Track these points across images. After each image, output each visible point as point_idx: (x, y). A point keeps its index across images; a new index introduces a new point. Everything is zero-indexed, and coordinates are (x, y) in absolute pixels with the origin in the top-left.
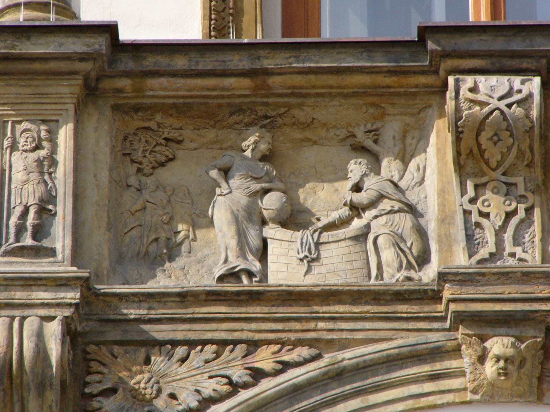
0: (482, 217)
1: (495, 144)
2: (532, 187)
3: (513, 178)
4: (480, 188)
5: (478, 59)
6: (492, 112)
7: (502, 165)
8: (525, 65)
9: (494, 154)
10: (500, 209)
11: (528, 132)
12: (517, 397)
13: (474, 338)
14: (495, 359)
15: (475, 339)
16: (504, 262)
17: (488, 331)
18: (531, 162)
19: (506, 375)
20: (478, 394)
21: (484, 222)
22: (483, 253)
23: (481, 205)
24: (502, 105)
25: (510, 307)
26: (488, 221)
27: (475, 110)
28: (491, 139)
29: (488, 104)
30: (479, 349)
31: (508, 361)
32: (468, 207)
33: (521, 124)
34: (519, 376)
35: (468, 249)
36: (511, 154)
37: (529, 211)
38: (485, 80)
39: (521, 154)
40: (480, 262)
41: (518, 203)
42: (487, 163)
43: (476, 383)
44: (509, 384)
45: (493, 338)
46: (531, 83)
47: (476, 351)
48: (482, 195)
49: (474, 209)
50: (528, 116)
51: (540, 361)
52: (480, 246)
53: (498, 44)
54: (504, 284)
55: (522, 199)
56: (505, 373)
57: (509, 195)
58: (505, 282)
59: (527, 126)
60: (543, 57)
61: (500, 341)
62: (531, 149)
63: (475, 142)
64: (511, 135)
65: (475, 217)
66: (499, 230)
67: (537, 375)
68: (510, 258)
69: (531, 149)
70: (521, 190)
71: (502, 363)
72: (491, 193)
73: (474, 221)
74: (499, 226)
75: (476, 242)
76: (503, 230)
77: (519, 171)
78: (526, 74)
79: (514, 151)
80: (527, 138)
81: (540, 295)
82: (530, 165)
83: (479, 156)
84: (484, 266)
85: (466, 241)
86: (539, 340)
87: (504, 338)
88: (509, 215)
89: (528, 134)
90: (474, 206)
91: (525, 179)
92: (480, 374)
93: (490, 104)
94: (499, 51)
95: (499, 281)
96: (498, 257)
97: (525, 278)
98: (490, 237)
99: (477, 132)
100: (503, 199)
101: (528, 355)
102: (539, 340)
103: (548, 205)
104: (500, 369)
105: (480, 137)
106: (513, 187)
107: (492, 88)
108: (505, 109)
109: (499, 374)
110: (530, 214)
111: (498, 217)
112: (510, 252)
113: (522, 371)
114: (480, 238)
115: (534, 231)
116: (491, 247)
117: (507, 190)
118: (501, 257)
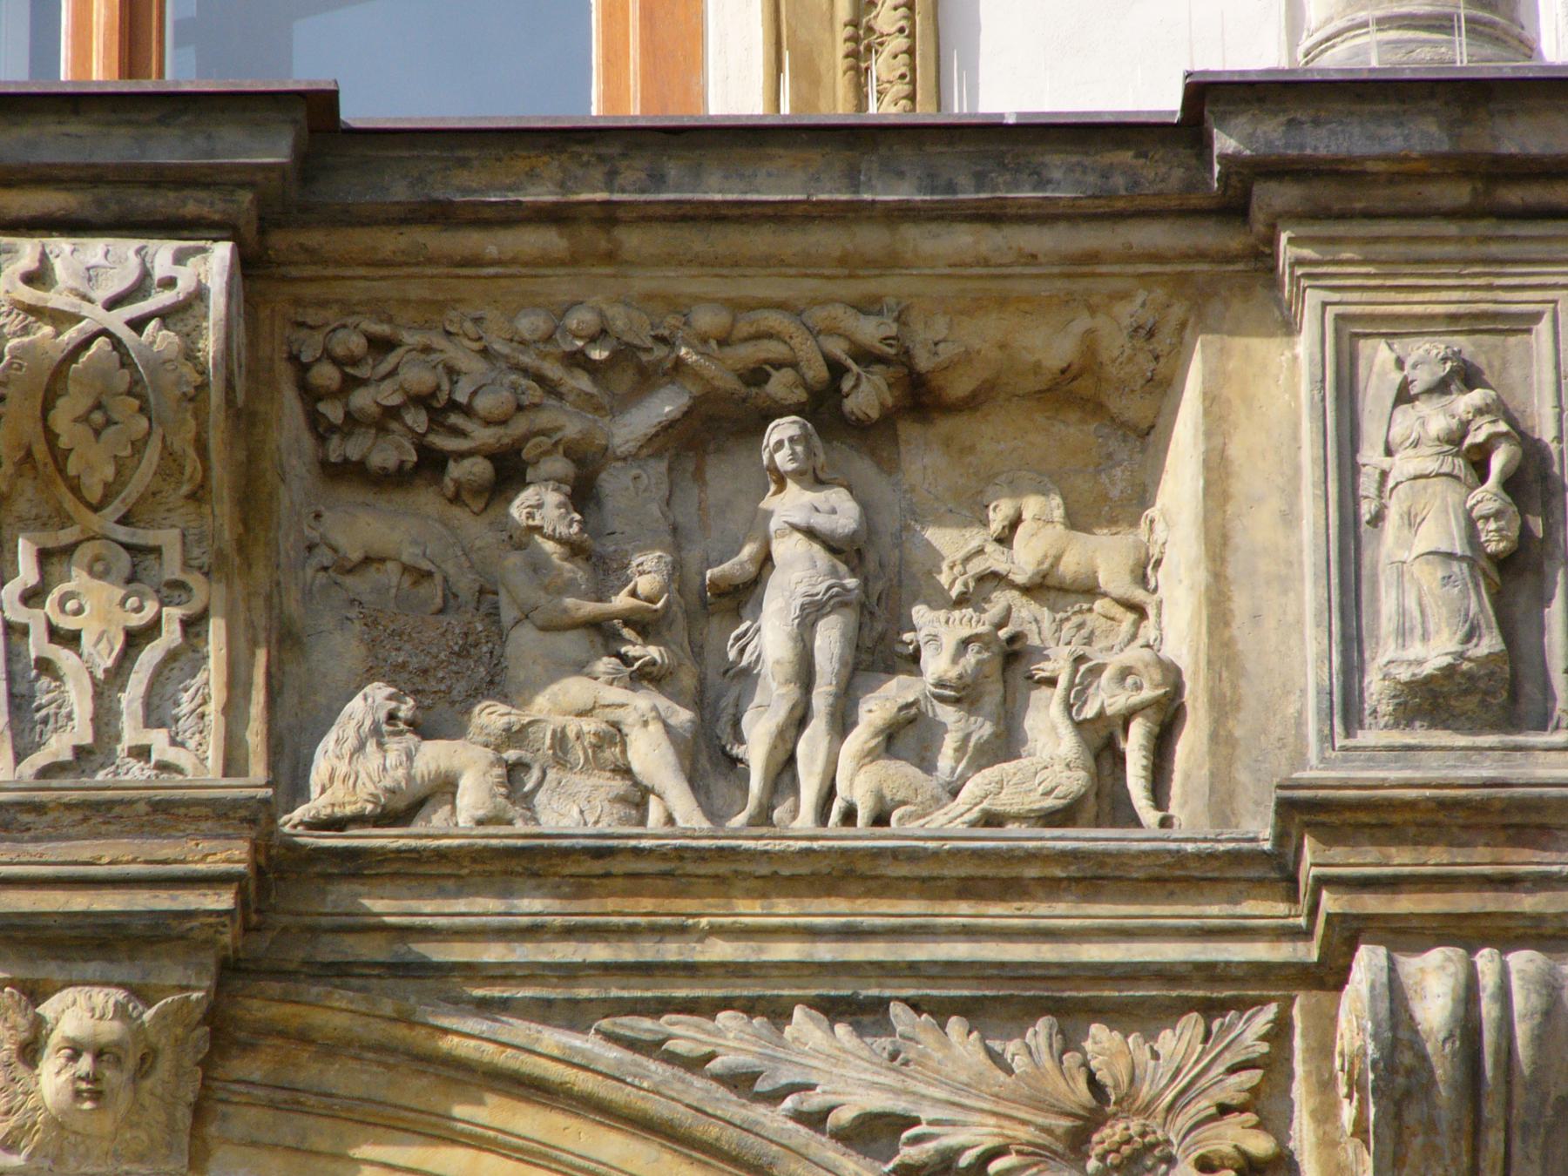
0: (59, 644)
1: (97, 433)
2: (205, 559)
3: (151, 533)
4: (55, 560)
5: (57, 189)
6: (86, 343)
7: (118, 493)
8: (191, 209)
9: (94, 464)
10: (109, 622)
11: (192, 399)
12: (130, 1161)
13: (7, 989)
14: (67, 1052)
15: (12, 995)
16: (116, 774)
17: (49, 970)
18: (202, 486)
19: (96, 1095)
20: (19, 1153)
21: (63, 657)
22: (58, 747)
23: (57, 609)
24: (117, 321)
25: (113, 902)
26: (74, 657)
27: (39, 334)
28: (84, 419)
29: (77, 318)
30: (23, 1023)
31: (105, 1058)
32: (17, 613)
33: (172, 377)
34: (135, 1101)
35: (14, 737)
36: (144, 462)
37: (193, 625)
38: (72, 253)
39: (170, 463)
40: (46, 772)
41: (163, 604)
42: (75, 489)
43: (13, 1121)
44: (107, 1123)
45: (65, 992)
46: (206, 260)
47: (13, 1027)
48: (61, 581)
49: (34, 619)
50: (190, 354)
51: (200, 1056)
52: (50, 726)
53: (114, 146)
54: (98, 835)
55: (176, 593)
56: (94, 1090)
57: (140, 581)
58: (103, 829)
59: (188, 383)
60: (241, 185)
61: (81, 1000)
62: (202, 449)
63: (39, 428)
64: (143, 409)
65: (38, 644)
66: (105, 681)
67: (191, 1098)
68: (132, 761)
69: (202, 449)
70: (172, 568)
71: (85, 1064)
72: (84, 575)
73: (33, 656)
74: (106, 671)
75: (38, 716)
76: (119, 682)
77: (169, 510)
78: (199, 235)
79: (152, 454)
80: (189, 416)
81: (201, 867)
82: (198, 495)
83: (51, 468)
84: (54, 783)
85: (10, 713)
86: (195, 995)
87: (96, 989)
88: (135, 639)
89: (190, 406)
90: (37, 611)
91: (184, 536)
92: (26, 1094)
93: (84, 318)
94: (118, 168)
95: (84, 828)
96: (99, 758)
97: (160, 818)
98: (79, 700)
99: (45, 399)
100: (119, 593)
101: (163, 1041)
102: (195, 995)
103: (249, 609)
104: (81, 1078)
105: (52, 413)
106: (152, 557)
107: (91, 274)
108: (125, 334)
109: (78, 1094)
110: (197, 635)
111: (103, 645)
112: (133, 743)
113: (147, 1084)
114: (50, 704)
115: (207, 683)
116: (81, 731)
117: (134, 566)
118: (109, 759)
